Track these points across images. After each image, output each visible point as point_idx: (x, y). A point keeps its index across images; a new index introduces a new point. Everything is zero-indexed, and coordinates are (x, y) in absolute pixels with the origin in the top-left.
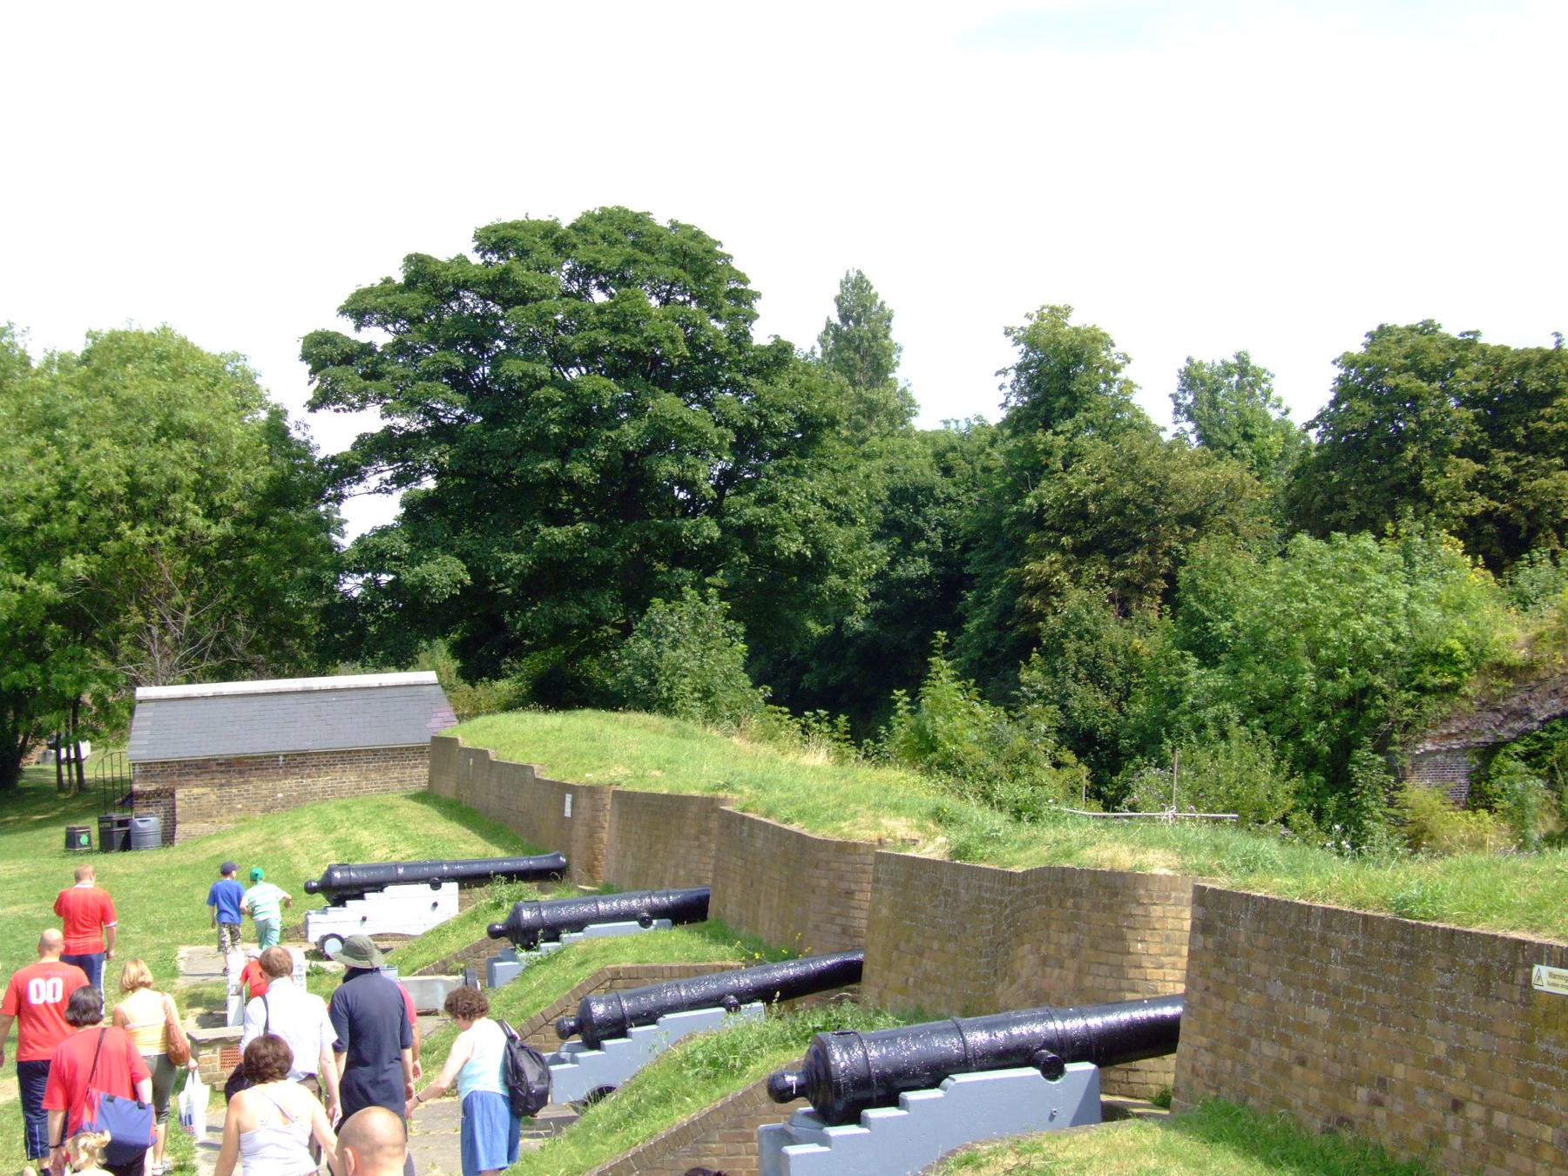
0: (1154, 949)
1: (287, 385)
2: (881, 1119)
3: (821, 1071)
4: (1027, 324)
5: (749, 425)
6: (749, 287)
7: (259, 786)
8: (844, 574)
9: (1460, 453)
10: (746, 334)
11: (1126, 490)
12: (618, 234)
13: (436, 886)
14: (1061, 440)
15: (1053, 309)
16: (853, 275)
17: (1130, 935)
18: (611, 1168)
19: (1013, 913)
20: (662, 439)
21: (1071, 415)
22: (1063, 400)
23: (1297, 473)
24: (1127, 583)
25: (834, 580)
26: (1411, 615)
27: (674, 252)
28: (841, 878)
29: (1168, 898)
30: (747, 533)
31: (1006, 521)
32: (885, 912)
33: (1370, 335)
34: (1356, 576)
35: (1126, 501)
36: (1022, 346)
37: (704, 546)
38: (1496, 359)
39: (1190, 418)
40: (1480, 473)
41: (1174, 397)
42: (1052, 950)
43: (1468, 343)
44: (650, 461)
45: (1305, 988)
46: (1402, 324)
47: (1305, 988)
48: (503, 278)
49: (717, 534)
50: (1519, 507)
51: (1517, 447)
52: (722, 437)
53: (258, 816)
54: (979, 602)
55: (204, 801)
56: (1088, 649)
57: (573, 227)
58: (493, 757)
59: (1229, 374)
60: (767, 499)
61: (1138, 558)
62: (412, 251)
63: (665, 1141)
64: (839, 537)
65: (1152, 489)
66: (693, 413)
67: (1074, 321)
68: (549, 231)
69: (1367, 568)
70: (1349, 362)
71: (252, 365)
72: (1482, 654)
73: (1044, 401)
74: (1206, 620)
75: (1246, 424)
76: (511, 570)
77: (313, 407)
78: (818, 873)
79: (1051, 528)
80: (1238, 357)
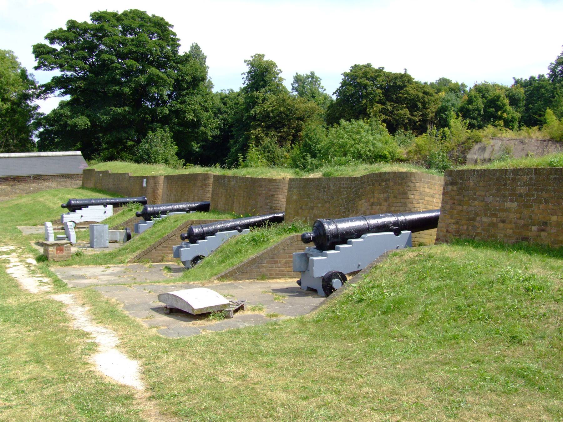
0: (417, 197)
1: (28, 61)
2: (343, 248)
3: (322, 233)
4: (251, 59)
5: (178, 79)
6: (177, 37)
7: (24, 186)
8: (205, 127)
9: (378, 102)
10: (177, 51)
11: (282, 109)
12: (136, 17)
13: (105, 206)
14: (261, 95)
15: (259, 55)
16: (194, 44)
17: (409, 192)
18: (229, 273)
19: (356, 191)
20: (153, 81)
21: (264, 87)
22: (262, 82)
23: (329, 108)
24: (281, 137)
25: (202, 128)
26: (373, 144)
27: (155, 23)
28: (270, 190)
29: (421, 180)
30: (177, 113)
31: (244, 118)
32: (295, 197)
33: (352, 67)
34: (358, 133)
35: (281, 113)
36: (250, 66)
37: (164, 116)
38: (388, 75)
39: (297, 91)
40: (383, 108)
41: (292, 84)
42: (375, 200)
43: (380, 70)
44: (149, 88)
45: (504, 197)
46: (361, 65)
47: (504, 197)
48: (101, 29)
49: (168, 112)
50: (394, 118)
51: (393, 101)
52: (171, 82)
53: (24, 195)
54: (235, 142)
55: (6, 190)
56: (271, 156)
57: (122, 14)
58: (110, 172)
59: (308, 78)
60: (183, 102)
61: (285, 129)
62: (70, 19)
63: (248, 263)
64: (204, 115)
65: (289, 109)
66: (160, 73)
67: (265, 59)
68: (115, 15)
69: (361, 130)
70: (346, 75)
71: (15, 54)
72: (394, 156)
73: (256, 82)
74: (310, 145)
75: (313, 93)
76: (103, 121)
77: (36, 68)
78: (262, 189)
79: (259, 120)
80: (311, 73)
